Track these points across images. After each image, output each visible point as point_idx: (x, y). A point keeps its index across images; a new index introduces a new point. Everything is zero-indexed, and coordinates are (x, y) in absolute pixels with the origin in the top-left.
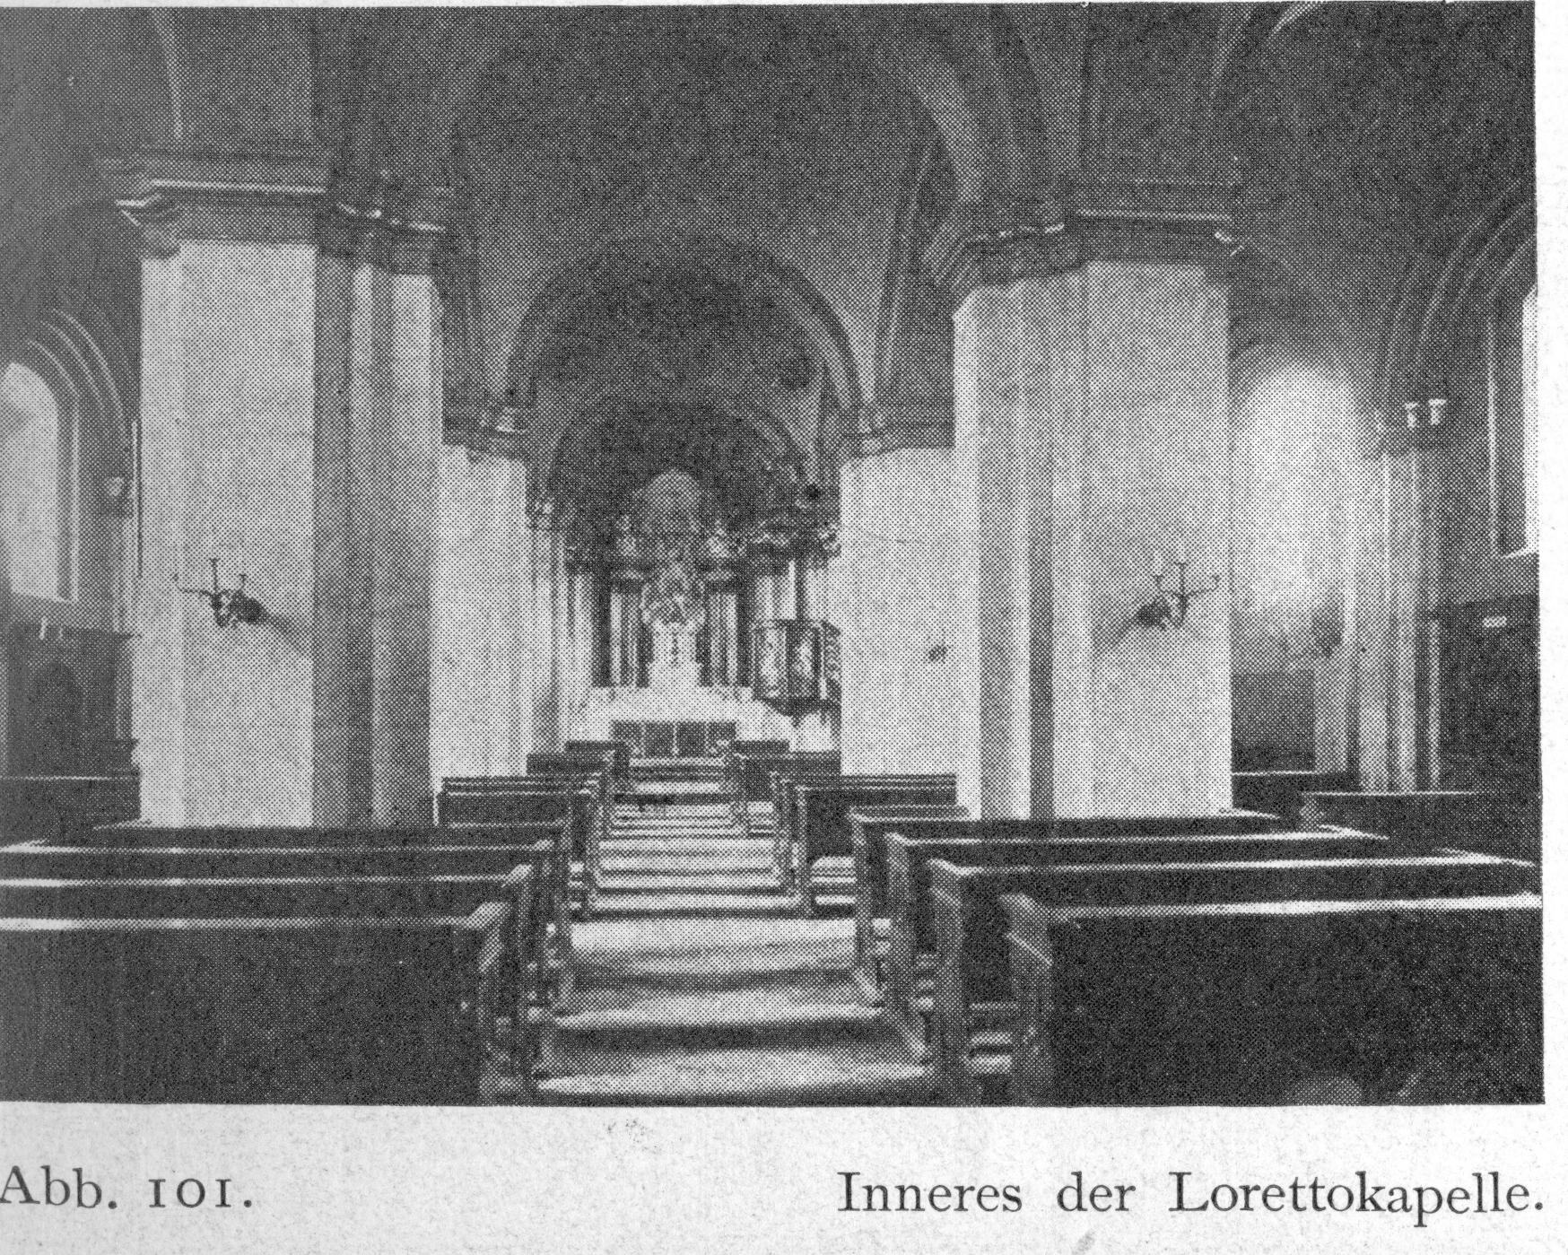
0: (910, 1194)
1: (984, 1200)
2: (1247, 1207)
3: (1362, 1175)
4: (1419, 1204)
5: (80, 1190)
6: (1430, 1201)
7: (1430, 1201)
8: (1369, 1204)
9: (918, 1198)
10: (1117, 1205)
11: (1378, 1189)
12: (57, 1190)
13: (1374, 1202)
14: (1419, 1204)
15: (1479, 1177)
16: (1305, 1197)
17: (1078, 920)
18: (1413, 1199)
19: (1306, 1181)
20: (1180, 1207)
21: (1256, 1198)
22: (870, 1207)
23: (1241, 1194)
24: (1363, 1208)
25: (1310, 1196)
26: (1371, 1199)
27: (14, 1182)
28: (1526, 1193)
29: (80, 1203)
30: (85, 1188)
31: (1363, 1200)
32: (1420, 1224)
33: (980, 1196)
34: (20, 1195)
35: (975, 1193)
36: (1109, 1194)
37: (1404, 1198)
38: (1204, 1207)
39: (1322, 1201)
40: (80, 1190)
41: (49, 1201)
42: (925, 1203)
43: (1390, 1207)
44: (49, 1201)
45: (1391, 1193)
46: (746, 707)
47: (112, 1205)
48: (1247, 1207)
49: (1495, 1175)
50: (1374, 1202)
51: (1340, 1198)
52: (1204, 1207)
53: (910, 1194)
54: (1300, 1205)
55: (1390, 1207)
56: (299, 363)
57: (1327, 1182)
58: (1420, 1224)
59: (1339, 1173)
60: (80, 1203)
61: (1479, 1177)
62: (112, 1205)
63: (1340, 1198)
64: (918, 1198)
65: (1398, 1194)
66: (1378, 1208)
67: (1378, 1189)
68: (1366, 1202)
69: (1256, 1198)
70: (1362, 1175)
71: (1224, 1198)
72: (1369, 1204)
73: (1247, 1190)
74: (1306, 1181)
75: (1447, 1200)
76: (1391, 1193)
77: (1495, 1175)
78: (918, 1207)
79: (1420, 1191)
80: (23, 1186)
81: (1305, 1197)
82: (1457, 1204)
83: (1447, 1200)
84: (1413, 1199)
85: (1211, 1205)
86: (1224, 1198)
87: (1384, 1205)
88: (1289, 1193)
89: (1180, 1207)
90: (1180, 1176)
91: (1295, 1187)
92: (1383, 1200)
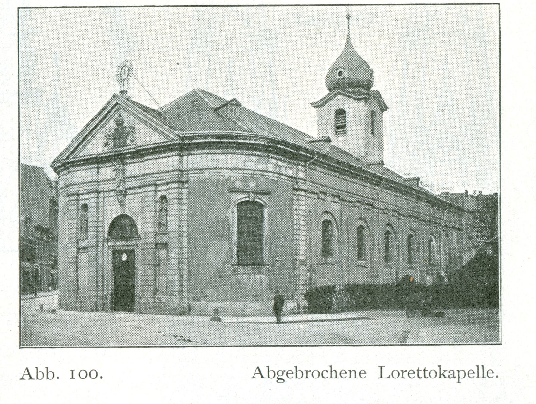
0: (353, 373)
1: (288, 375)
2: (403, 377)
3: (440, 366)
4: (457, 376)
5: (48, 374)
6: (462, 374)
7: (462, 374)
8: (442, 376)
9: (336, 374)
10: (330, 376)
11: (445, 371)
12: (40, 375)
13: (444, 375)
14: (457, 376)
15: (478, 366)
16: (421, 374)
17: (50, 291)
18: (456, 374)
19: (422, 369)
20: (381, 377)
21: (406, 374)
22: (331, 377)
23: (401, 373)
24: (440, 377)
25: (425, 374)
26: (443, 374)
27: (258, 372)
28: (493, 373)
29: (48, 378)
30: (270, 372)
31: (440, 375)
32: (459, 382)
33: (409, 373)
34: (28, 377)
35: (407, 373)
36: (346, 373)
37: (454, 374)
38: (389, 377)
39: (427, 375)
40: (48, 374)
41: (269, 377)
42: (338, 375)
43: (449, 376)
44: (269, 377)
45: (449, 372)
46: (384, 228)
47: (58, 378)
48: (403, 377)
49: (483, 366)
50: (444, 375)
51: (433, 374)
52: (389, 377)
53: (353, 373)
54: (420, 376)
55: (449, 377)
56: (219, 158)
57: (429, 369)
58: (459, 382)
59: (432, 366)
60: (48, 378)
61: (478, 366)
62: (58, 378)
63: (433, 374)
64: (336, 374)
65: (452, 372)
66: (445, 377)
67: (445, 371)
68: (441, 375)
69: (406, 374)
70: (440, 366)
71: (395, 374)
72: (442, 376)
73: (307, 372)
74: (422, 369)
75: (467, 374)
76: (449, 372)
77: (483, 366)
78: (336, 377)
79: (459, 371)
80: (260, 373)
81: (421, 374)
82: (471, 375)
83: (467, 374)
84: (456, 374)
85: (391, 376)
86: (395, 374)
87: (447, 376)
88: (416, 373)
89: (381, 377)
90: (381, 367)
91: (418, 370)
92: (446, 374)
